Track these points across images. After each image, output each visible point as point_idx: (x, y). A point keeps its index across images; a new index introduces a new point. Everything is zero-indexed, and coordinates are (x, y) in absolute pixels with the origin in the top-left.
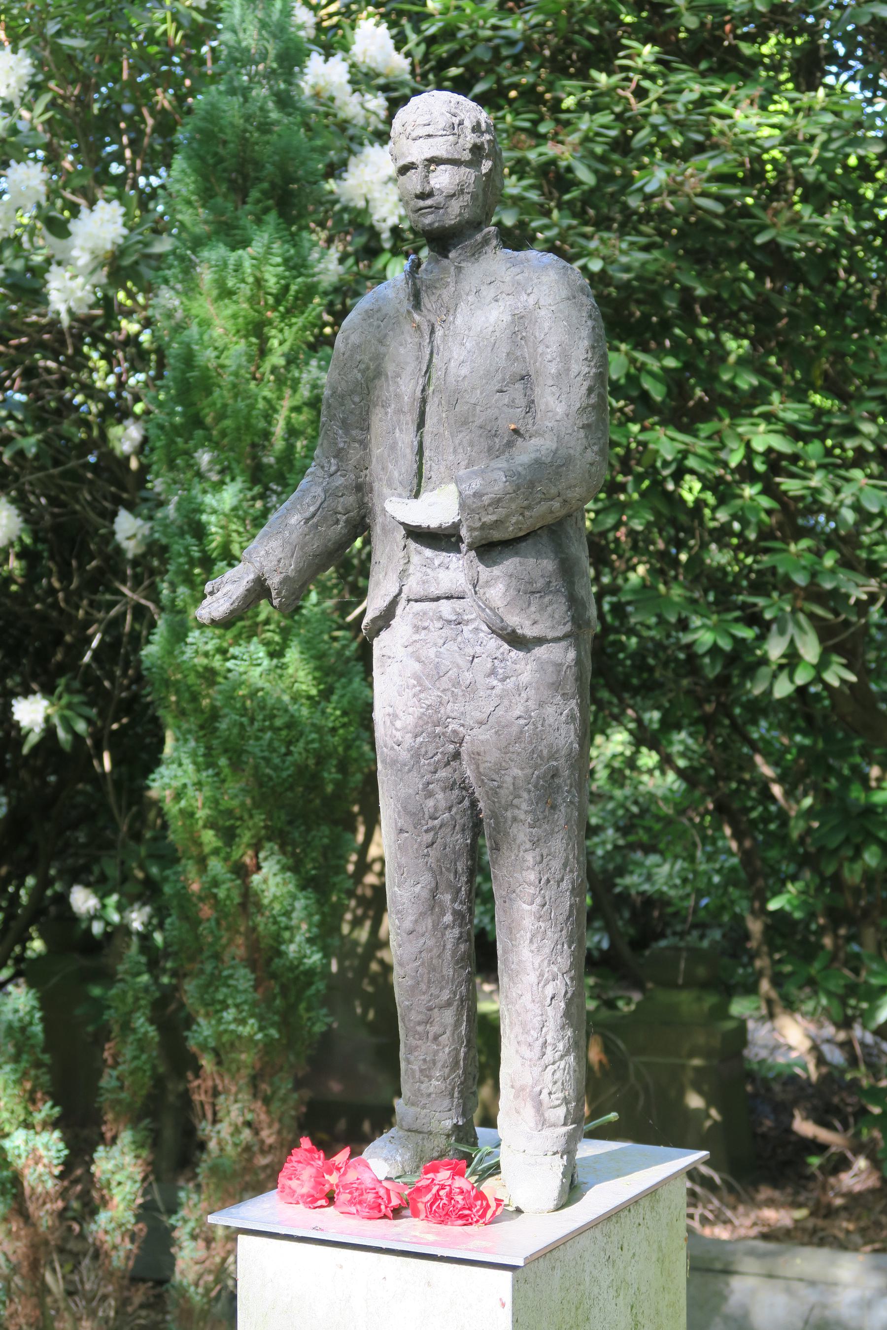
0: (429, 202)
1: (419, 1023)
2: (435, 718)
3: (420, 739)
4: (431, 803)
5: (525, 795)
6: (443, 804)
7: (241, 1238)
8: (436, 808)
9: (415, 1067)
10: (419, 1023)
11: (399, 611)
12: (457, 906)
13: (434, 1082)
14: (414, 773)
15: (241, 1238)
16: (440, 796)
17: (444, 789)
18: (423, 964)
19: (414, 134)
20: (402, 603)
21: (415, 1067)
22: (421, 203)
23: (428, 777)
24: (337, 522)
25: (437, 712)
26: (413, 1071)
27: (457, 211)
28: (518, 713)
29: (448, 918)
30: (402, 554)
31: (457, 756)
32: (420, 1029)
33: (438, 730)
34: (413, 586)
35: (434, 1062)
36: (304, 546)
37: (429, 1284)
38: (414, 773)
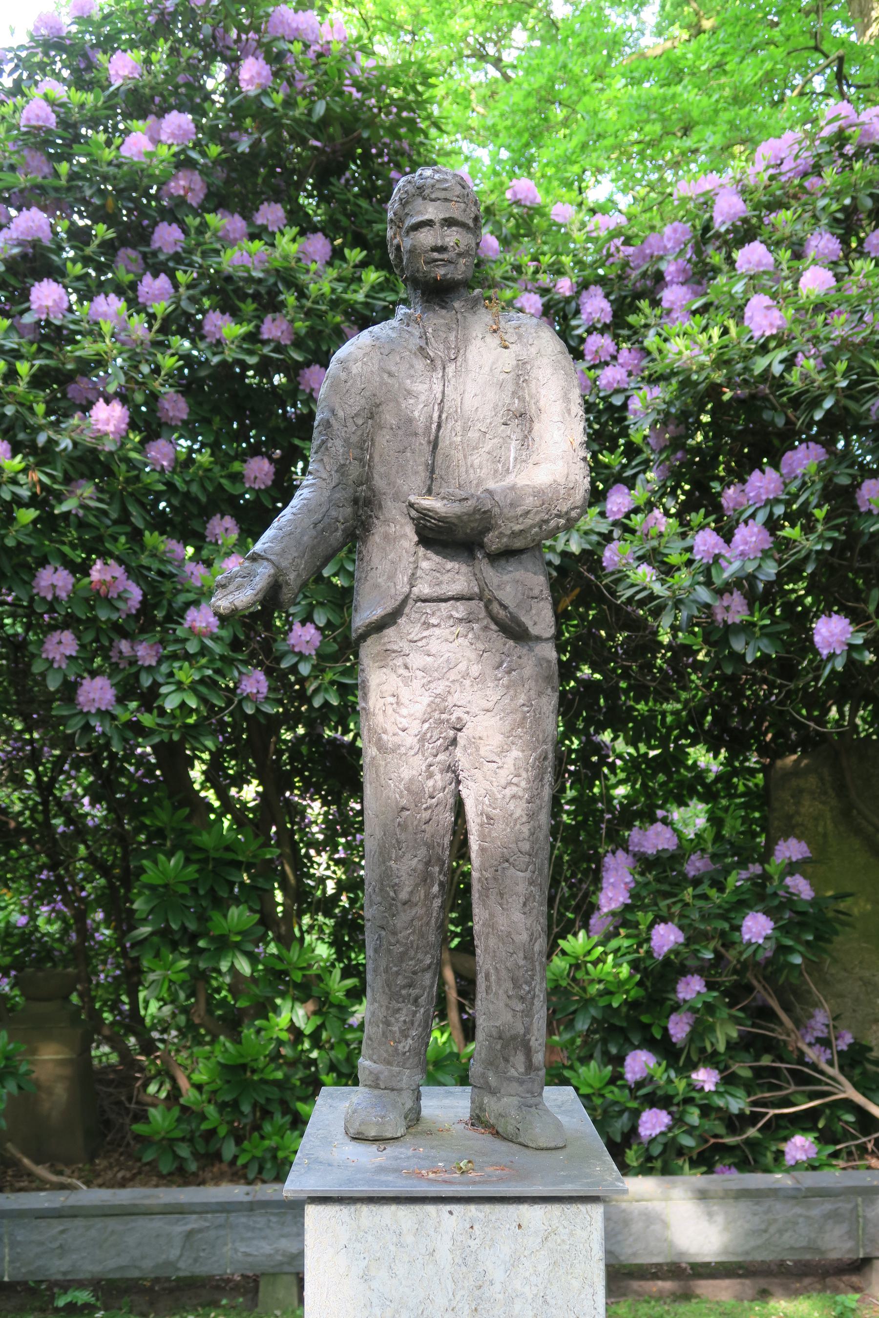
0: (445, 256)
1: (404, 987)
2: (442, 706)
3: (426, 725)
4: (430, 783)
5: (524, 775)
6: (440, 784)
7: (311, 1211)
8: (434, 787)
9: (395, 1029)
10: (404, 987)
11: (407, 610)
12: (442, 878)
13: (410, 1041)
14: (420, 755)
15: (311, 1211)
16: (438, 777)
17: (441, 772)
18: (413, 933)
19: (433, 196)
20: (411, 602)
21: (395, 1029)
22: (436, 255)
23: (430, 759)
24: (336, 530)
25: (444, 700)
26: (393, 1033)
27: (463, 268)
28: (521, 701)
29: (435, 889)
30: (412, 559)
31: (454, 742)
32: (404, 992)
33: (443, 716)
34: (424, 589)
35: (412, 1023)
36: (313, 548)
37: (520, 1226)
38: (420, 755)
